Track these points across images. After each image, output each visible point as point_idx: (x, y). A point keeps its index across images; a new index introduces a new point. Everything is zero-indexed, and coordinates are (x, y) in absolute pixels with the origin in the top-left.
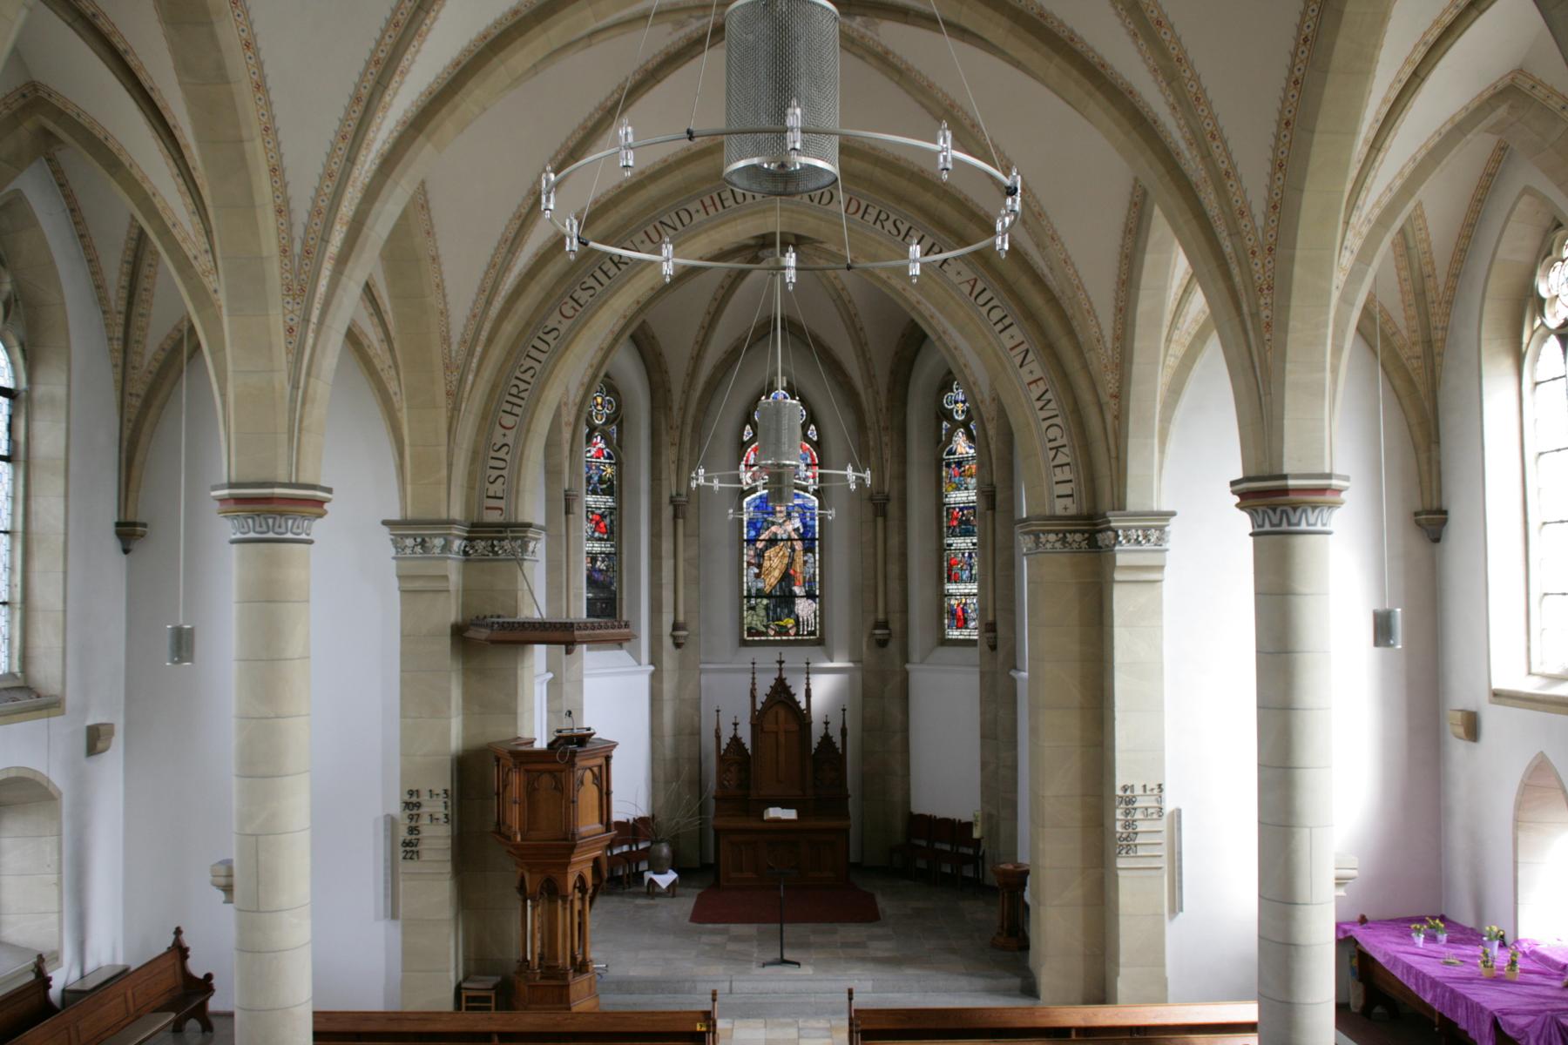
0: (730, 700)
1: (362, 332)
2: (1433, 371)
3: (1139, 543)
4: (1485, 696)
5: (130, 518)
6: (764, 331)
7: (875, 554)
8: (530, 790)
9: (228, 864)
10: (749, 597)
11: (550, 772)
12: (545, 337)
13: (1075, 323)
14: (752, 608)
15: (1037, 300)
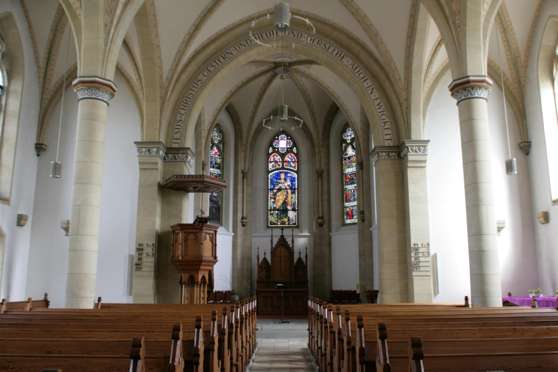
0: (263, 245)
1: (131, 77)
2: (522, 92)
3: (416, 152)
4: (550, 203)
5: (41, 142)
6: (276, 112)
7: (318, 192)
8: (186, 240)
9: (68, 221)
10: (271, 210)
11: (193, 233)
12: (197, 83)
13: (390, 75)
14: (272, 214)
15: (376, 68)
